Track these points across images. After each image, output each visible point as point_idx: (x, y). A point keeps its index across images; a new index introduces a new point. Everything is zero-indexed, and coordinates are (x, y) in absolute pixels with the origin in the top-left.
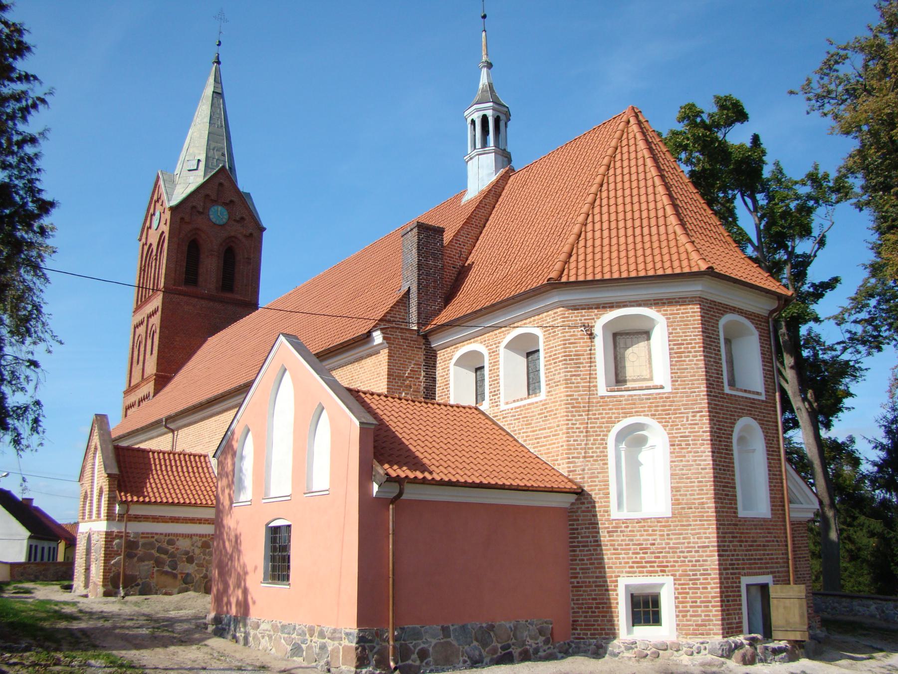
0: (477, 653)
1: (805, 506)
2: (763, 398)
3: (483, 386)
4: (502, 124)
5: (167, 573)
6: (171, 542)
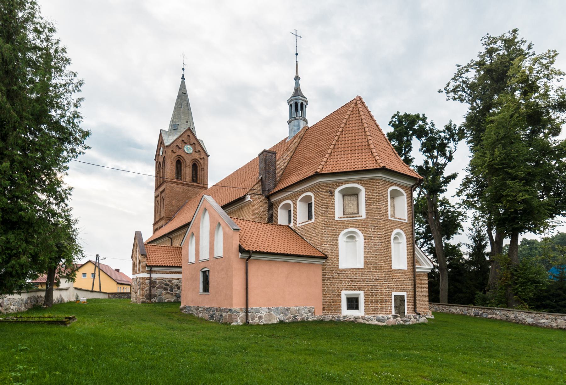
1: (427, 267)
2: (406, 221)
4: (304, 106)
5: (169, 293)
6: (170, 281)
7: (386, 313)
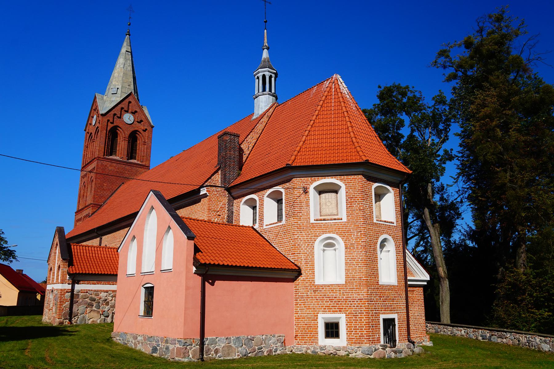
0: (245, 351)
2: (395, 225)
3: (256, 216)
7: (373, 342)
